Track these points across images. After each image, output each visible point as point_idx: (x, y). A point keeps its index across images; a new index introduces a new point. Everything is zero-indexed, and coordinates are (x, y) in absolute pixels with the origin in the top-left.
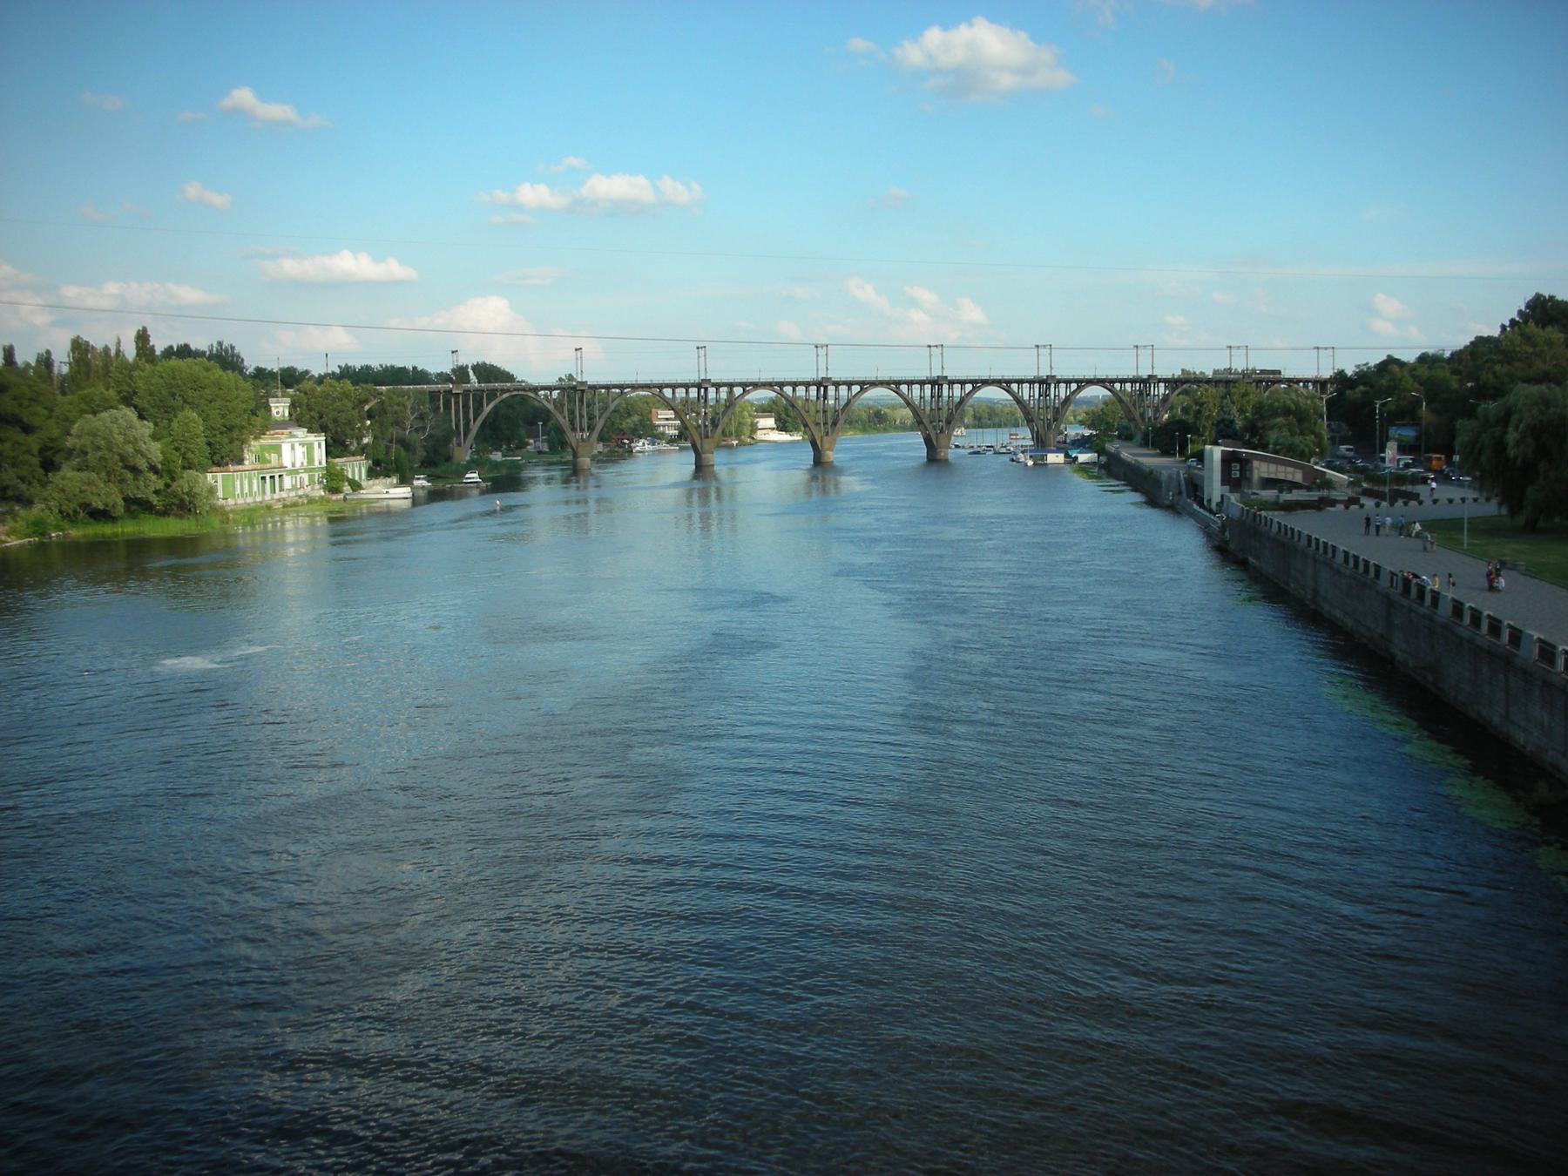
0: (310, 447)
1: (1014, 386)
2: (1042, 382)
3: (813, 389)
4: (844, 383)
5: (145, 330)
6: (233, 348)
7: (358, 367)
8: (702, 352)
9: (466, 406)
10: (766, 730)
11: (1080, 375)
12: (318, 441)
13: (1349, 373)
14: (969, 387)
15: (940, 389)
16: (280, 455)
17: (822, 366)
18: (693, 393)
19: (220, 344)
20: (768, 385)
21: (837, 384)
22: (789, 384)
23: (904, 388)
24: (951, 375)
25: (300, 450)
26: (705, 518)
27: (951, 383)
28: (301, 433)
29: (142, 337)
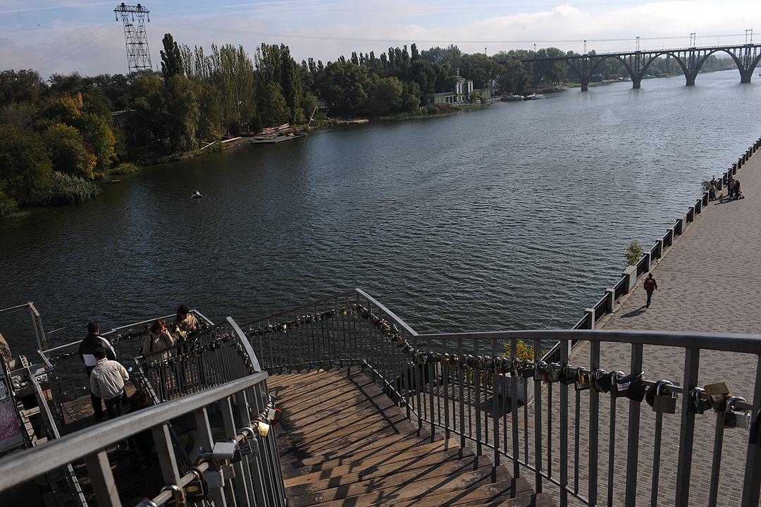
12: (470, 85)
20: (722, 49)
22: (732, 48)
29: (413, 47)
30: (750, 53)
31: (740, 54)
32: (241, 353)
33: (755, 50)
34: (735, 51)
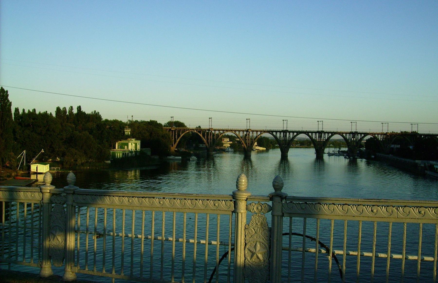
0: (136, 144)
1: (310, 134)
2: (318, 132)
3: (282, 133)
4: (242, 131)
5: (80, 106)
6: (99, 113)
7: (140, 121)
8: (210, 120)
9: (175, 133)
10: (353, 246)
11: (332, 130)
13: (37, 112)
14: (295, 134)
15: (286, 134)
16: (128, 147)
17: (210, 125)
18: (245, 133)
19: (95, 111)
21: (253, 131)
23: (274, 133)
24: (289, 129)
25: (134, 145)
26: (248, 170)
27: (290, 132)
28: (133, 140)
30: (286, 136)
31: (280, 137)
32: (403, 231)
33: (289, 134)
34: (276, 134)
